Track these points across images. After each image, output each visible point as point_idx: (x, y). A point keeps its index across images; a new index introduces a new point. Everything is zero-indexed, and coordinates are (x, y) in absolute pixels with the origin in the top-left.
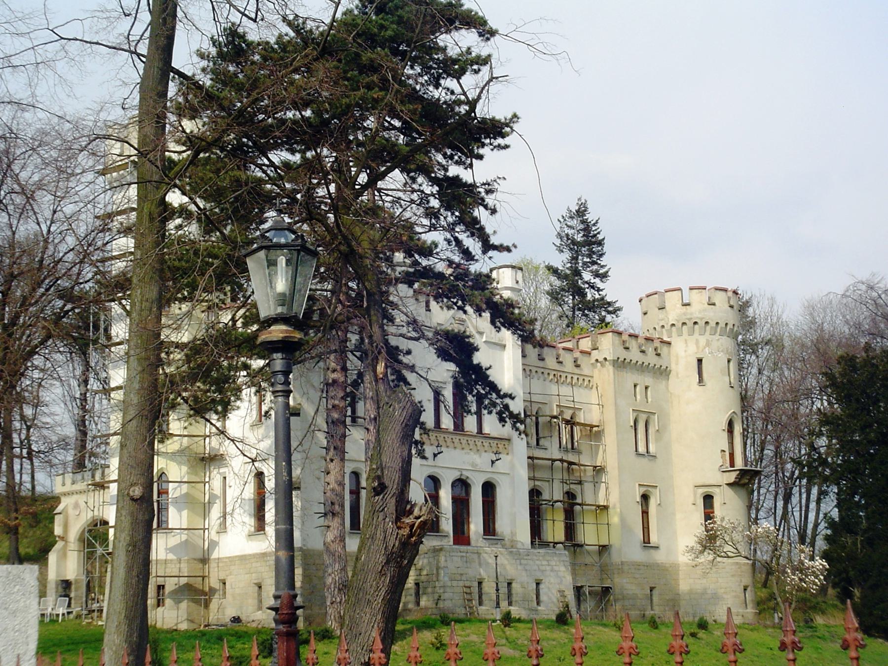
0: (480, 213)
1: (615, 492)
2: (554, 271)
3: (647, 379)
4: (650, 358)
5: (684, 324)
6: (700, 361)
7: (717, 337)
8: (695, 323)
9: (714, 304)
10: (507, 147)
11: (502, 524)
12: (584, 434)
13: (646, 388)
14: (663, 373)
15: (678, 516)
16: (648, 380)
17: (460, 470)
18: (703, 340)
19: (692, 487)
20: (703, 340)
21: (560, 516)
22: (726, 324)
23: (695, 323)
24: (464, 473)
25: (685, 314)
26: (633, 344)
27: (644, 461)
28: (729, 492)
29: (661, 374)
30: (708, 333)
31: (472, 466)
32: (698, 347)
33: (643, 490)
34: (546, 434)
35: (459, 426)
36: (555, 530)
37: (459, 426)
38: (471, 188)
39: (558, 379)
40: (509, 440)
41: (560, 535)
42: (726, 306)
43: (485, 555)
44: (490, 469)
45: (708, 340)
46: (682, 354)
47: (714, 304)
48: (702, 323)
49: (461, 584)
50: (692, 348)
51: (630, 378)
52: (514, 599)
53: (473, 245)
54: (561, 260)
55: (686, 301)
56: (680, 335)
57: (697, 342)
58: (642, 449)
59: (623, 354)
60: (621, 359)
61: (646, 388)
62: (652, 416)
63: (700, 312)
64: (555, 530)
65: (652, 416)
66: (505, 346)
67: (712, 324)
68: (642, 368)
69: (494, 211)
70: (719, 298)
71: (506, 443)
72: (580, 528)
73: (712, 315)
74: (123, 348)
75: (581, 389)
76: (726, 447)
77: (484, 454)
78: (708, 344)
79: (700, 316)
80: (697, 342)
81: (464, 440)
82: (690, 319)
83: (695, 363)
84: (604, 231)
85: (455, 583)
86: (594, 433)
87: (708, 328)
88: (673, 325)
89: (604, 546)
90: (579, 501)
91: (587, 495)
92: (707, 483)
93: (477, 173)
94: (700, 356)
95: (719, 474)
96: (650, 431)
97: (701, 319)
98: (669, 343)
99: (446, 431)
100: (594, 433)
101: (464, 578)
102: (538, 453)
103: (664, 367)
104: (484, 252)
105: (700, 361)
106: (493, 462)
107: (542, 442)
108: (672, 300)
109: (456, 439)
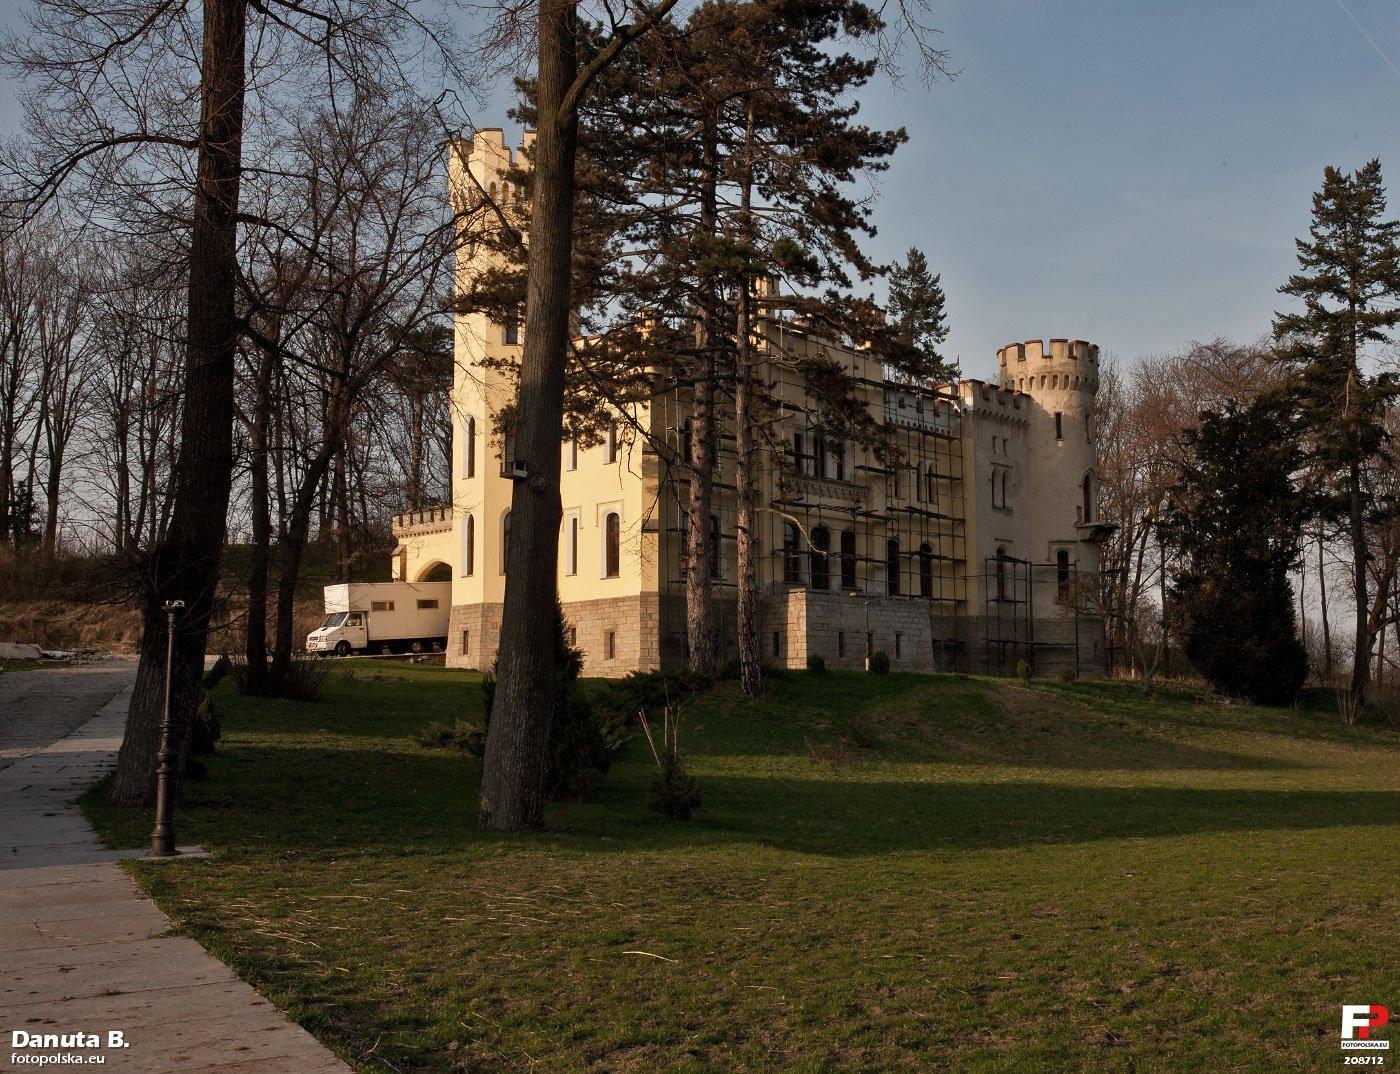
0: (857, 235)
3: (1006, 432)
4: (1010, 411)
10: (886, 167)
13: (1005, 441)
19: (1046, 543)
21: (917, 569)
25: (1045, 367)
26: (993, 396)
27: (1001, 515)
28: (1083, 549)
33: (999, 544)
35: (893, 587)
36: (911, 584)
37: (893, 587)
38: (847, 206)
41: (917, 591)
53: (850, 270)
55: (1046, 353)
58: (999, 503)
61: (1005, 441)
63: (1060, 365)
64: (911, 584)
68: (1003, 420)
69: (873, 232)
72: (936, 582)
74: (913, 379)
76: (1082, 504)
81: (824, 486)
89: (960, 601)
90: (936, 552)
93: (853, 189)
96: (1007, 485)
97: (1062, 373)
99: (807, 477)
102: (895, 503)
104: (864, 278)
108: (1033, 352)
109: (817, 485)
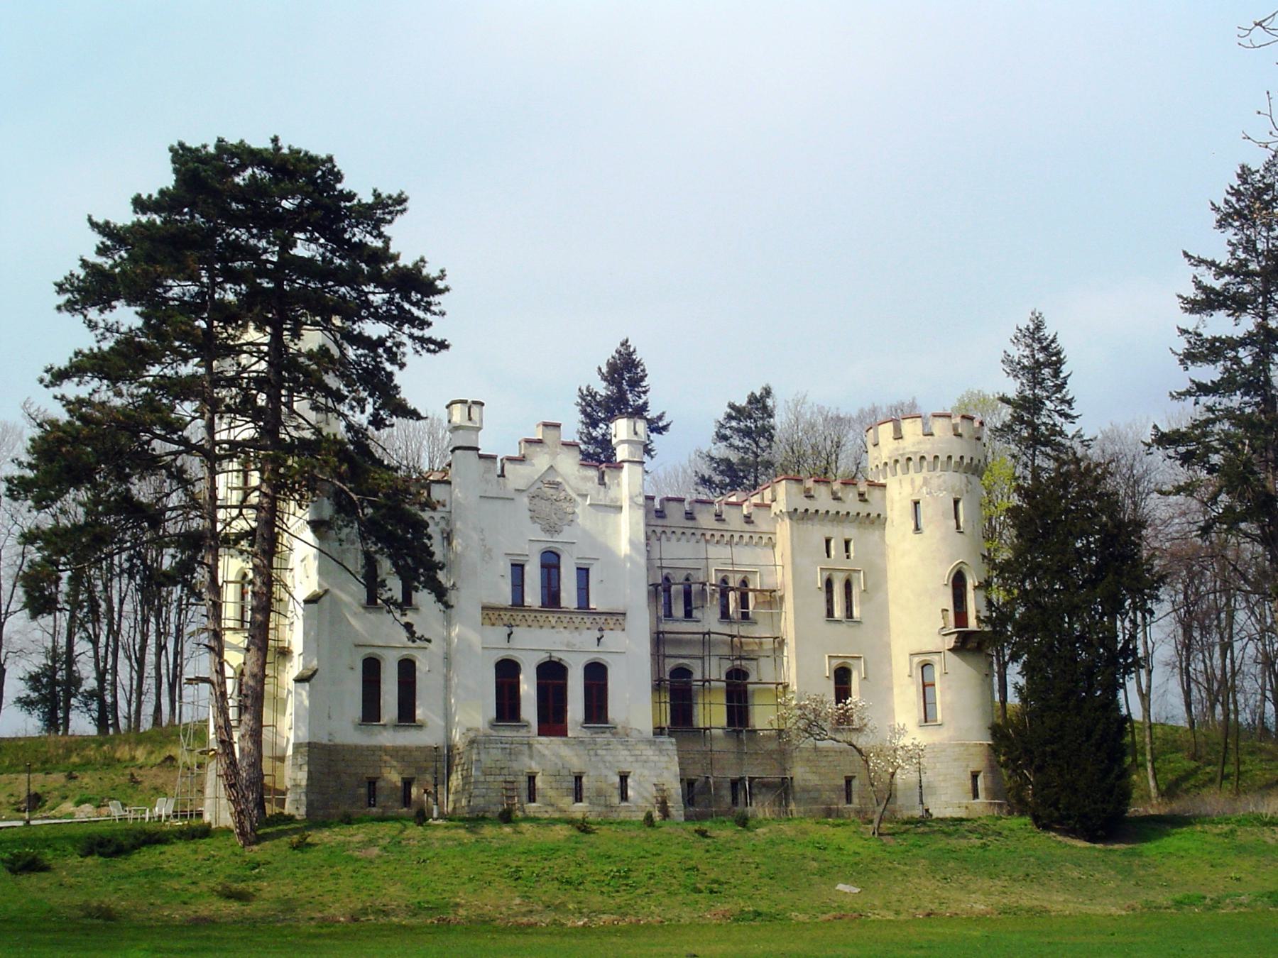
1: (796, 670)
2: (1004, 400)
4: (851, 503)
5: (897, 461)
6: (916, 503)
7: (938, 472)
8: (909, 459)
9: (932, 435)
11: (615, 710)
12: (760, 600)
13: (847, 543)
14: (877, 521)
15: (896, 691)
16: (849, 532)
17: (546, 651)
18: (919, 479)
20: (919, 479)
22: (950, 457)
23: (909, 459)
24: (554, 654)
25: (897, 449)
28: (953, 659)
29: (872, 523)
30: (925, 470)
31: (567, 645)
32: (913, 488)
34: (699, 603)
39: (704, 536)
40: (624, 614)
42: (950, 434)
43: (539, 747)
44: (506, 645)
45: (925, 479)
46: (897, 497)
47: (932, 435)
48: (916, 459)
49: (501, 778)
50: (907, 489)
51: (817, 532)
52: (585, 793)
54: (1012, 387)
56: (895, 474)
57: (913, 481)
59: (803, 504)
60: (801, 510)
62: (855, 575)
65: (855, 575)
66: (621, 508)
67: (930, 458)
70: (939, 427)
71: (620, 618)
73: (927, 447)
75: (758, 550)
77: (586, 632)
78: (926, 482)
79: (914, 450)
80: (913, 481)
82: (902, 455)
83: (910, 506)
84: (1066, 344)
85: (490, 779)
86: (772, 599)
87: (925, 463)
88: (886, 464)
91: (761, 672)
92: (924, 650)
94: (916, 498)
95: (939, 639)
97: (915, 453)
98: (884, 486)
100: (772, 599)
101: (505, 771)
102: (668, 626)
103: (874, 515)
105: (916, 503)
106: (599, 640)
107: (695, 613)
